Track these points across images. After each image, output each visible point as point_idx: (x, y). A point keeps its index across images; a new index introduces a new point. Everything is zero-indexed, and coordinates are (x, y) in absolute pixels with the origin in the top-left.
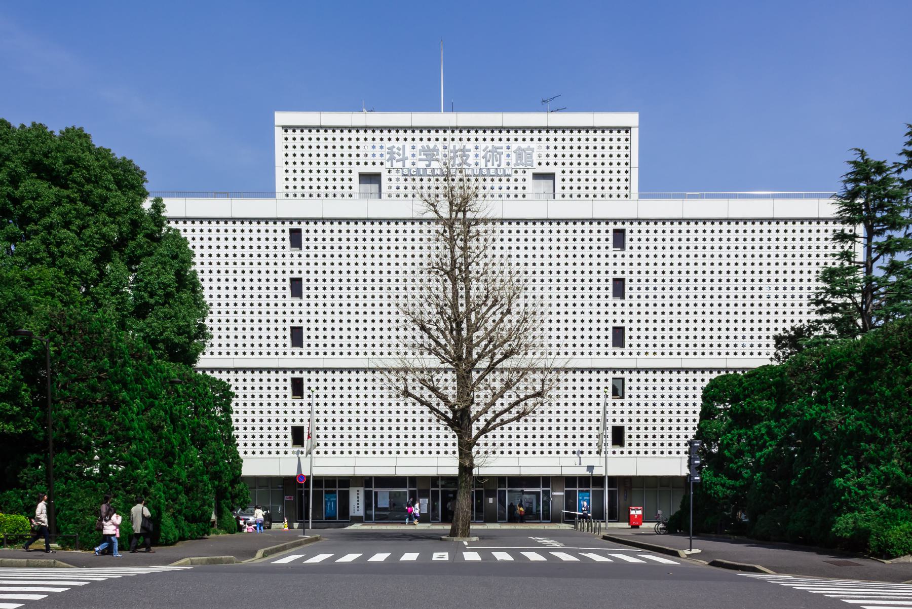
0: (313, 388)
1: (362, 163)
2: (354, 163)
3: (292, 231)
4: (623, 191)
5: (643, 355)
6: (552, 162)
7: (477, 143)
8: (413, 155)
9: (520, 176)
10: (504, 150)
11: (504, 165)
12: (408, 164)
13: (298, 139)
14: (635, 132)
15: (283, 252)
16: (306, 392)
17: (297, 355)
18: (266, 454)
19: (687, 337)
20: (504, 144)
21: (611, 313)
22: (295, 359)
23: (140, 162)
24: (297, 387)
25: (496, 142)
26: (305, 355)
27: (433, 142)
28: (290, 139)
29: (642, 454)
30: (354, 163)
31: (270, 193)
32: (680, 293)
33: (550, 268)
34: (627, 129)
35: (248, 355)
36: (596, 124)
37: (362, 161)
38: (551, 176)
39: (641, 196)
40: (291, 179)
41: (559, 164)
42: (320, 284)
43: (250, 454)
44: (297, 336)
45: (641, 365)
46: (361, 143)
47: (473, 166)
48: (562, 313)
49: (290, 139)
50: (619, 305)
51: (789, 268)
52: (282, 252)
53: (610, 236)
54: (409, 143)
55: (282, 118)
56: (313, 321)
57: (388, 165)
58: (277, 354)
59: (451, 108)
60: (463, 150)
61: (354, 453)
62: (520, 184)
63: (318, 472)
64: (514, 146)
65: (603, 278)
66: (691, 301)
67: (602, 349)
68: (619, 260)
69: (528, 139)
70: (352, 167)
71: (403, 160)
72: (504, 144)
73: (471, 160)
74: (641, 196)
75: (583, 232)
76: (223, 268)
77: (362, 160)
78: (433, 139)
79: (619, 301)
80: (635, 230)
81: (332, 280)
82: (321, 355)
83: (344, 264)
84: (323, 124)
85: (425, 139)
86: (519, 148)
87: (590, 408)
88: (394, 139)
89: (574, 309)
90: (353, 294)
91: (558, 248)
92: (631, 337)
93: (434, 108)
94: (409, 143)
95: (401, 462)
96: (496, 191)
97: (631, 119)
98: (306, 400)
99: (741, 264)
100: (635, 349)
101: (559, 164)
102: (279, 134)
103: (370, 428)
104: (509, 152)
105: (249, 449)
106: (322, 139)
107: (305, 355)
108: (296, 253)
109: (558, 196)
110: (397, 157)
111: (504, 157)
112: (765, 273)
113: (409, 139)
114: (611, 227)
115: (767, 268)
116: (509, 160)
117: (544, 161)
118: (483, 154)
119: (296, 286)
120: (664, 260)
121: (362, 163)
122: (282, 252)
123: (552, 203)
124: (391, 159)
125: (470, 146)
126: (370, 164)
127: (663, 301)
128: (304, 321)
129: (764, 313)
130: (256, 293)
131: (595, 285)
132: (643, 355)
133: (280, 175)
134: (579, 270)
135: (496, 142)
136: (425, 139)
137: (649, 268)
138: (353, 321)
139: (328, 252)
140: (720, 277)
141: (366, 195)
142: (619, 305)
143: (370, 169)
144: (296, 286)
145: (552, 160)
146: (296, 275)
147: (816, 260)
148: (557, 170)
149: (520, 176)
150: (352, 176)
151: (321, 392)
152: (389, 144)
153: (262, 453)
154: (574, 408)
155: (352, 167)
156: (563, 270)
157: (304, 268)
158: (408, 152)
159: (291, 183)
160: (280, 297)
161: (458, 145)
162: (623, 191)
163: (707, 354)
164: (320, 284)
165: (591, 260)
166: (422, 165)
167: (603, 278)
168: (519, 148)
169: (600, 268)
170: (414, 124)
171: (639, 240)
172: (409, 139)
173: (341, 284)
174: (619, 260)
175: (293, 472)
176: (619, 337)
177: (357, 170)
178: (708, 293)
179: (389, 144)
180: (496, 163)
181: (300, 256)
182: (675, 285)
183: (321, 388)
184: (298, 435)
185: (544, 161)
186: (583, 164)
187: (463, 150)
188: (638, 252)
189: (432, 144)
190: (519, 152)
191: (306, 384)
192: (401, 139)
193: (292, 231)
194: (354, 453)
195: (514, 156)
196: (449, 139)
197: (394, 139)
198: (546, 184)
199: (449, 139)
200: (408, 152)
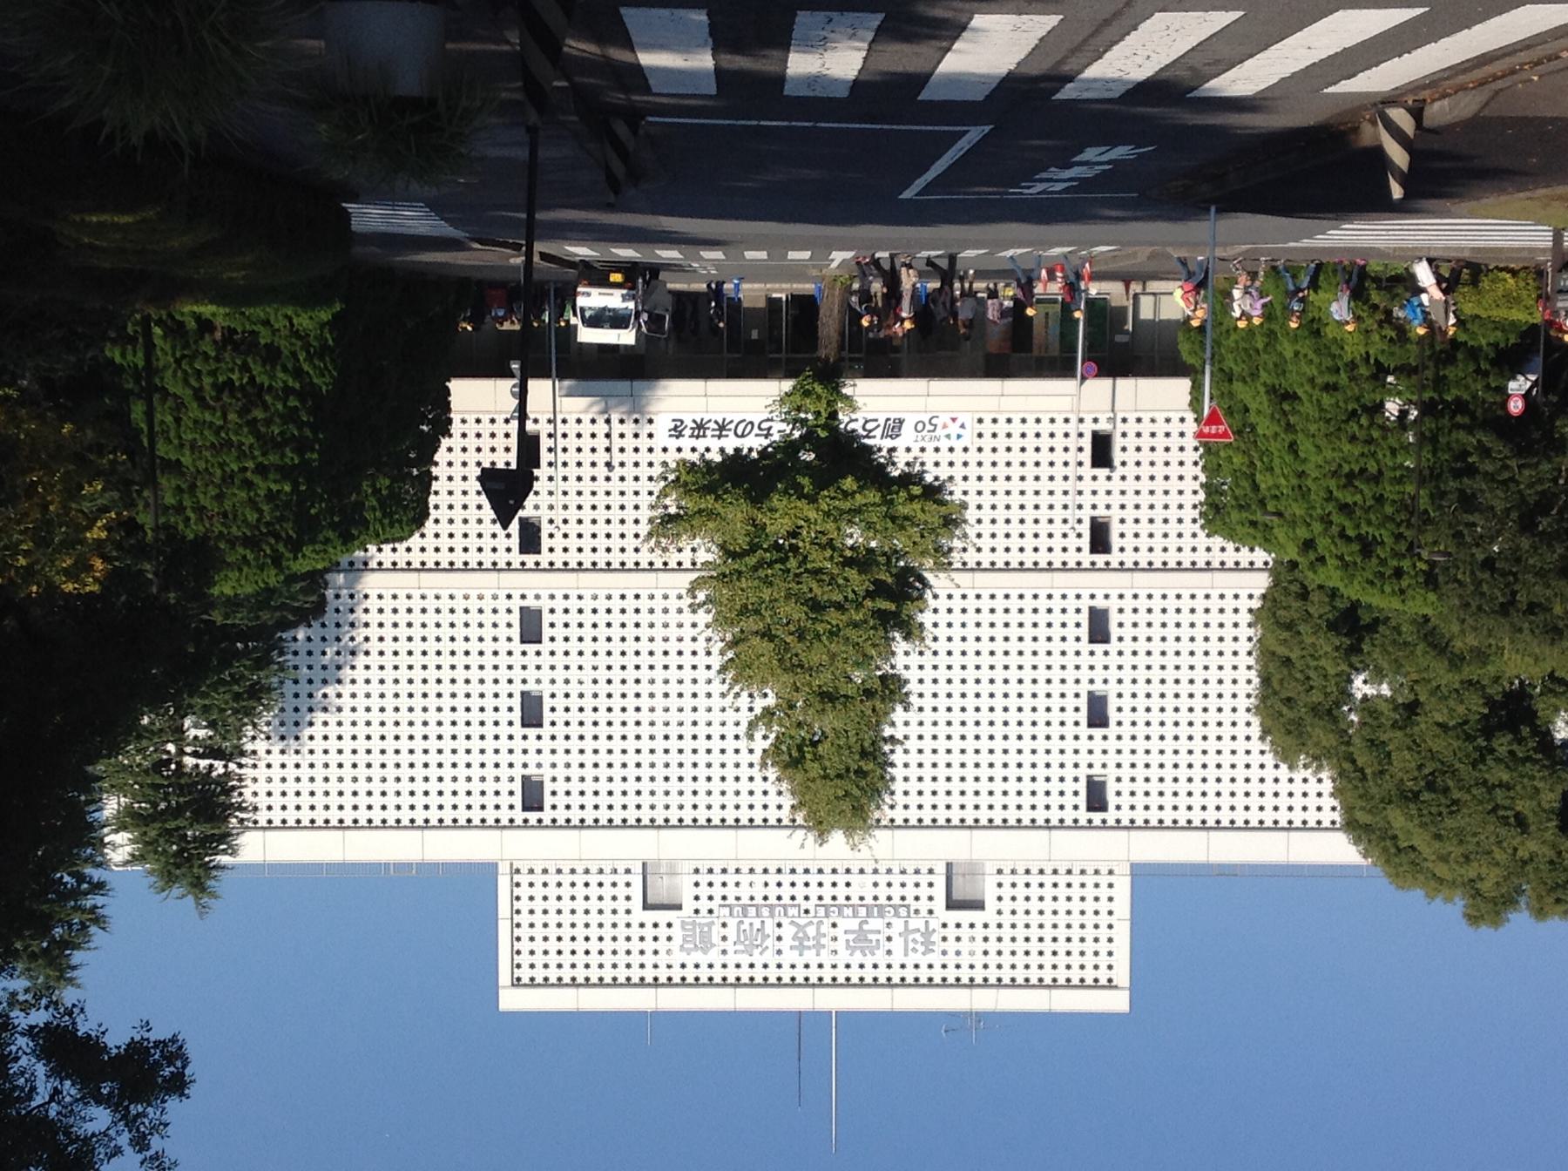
0: (1072, 535)
1: (979, 926)
2: (993, 926)
3: (1103, 807)
4: (524, 879)
5: (488, 594)
6: (965, 930)
7: (723, 959)
8: (889, 939)
9: (704, 905)
10: (731, 949)
11: (732, 923)
12: (898, 925)
13: (608, 966)
14: (504, 977)
15: (1119, 772)
16: (1085, 529)
17: (1100, 594)
18: (1160, 417)
19: (978, 695)
20: (731, 959)
21: (1228, 668)
22: (1101, 587)
23: (1541, 925)
24: (1100, 538)
25: (800, 963)
26: (1085, 594)
27: (910, 964)
28: (1103, 967)
29: (485, 419)
30: (993, 926)
31: (1141, 873)
32: (963, 703)
33: (1034, 745)
34: (517, 983)
35: (1171, 594)
36: (572, 991)
37: (979, 932)
38: (952, 905)
39: (495, 865)
40: (1007, 899)
41: (635, 925)
42: (1141, 716)
43: (1175, 417)
44: (531, 628)
45: (1045, 578)
46: (979, 960)
47: (785, 921)
48: (1099, 668)
49: (1103, 967)
50: (1098, 681)
51: (956, 786)
52: (1122, 772)
53: (548, 800)
54: (896, 960)
55: (1118, 1002)
56: (503, 653)
57: (935, 924)
58: (552, 597)
59: (820, 1018)
60: (801, 949)
61: (1002, 419)
62: (704, 891)
63: (1066, 386)
64: (714, 956)
65: (1126, 727)
66: (1156, 688)
67: (559, 604)
68: (1097, 759)
69: (690, 966)
70: (995, 919)
71: (907, 930)
72: (731, 959)
73: (788, 931)
74: (495, 865)
75: (1147, 808)
76: (1055, 744)
77: (979, 932)
78: (910, 968)
79: (1098, 687)
80: (1069, 811)
81: (1006, 723)
82: (1143, 594)
83: (998, 751)
84: (1045, 992)
85: (869, 966)
86: (705, 951)
87: (594, 500)
88: (923, 967)
89: (1178, 674)
90: (1141, 699)
91: (1062, 779)
92: (509, 625)
93: (848, 1019)
94: (896, 960)
95: (992, 403)
96: (759, 879)
97: (511, 1000)
98: (1086, 514)
99: (376, 752)
100: (502, 604)
101: (635, 925)
102: (1122, 975)
103: (987, 464)
104: (723, 946)
105: (1175, 428)
106: (580, 966)
107: (1085, 594)
108: (1097, 770)
109: (941, 869)
110: (918, 936)
111: (732, 937)
112: (1013, 737)
113: (896, 966)
114: (547, 816)
115: (358, 745)
116: (724, 931)
117: (663, 932)
118: (769, 942)
119: (1098, 715)
120: (1020, 716)
121: (979, 926)
122: (1122, 772)
123: (650, 854)
124: (928, 933)
125: (789, 957)
126: (663, 925)
127: (1063, 688)
128: (517, 653)
129: (1085, 668)
130: (1213, 703)
131: (489, 716)
132: (488, 594)
133: (1123, 906)
134: (1169, 742)
135: (800, 963)
136: (869, 966)
137: (1002, 744)
138: (956, 653)
139: (702, 772)
140: (624, 730)
141: (974, 870)
142: (1098, 681)
143: (965, 916)
144: (1098, 715)
145: (649, 932)
146: (532, 732)
147: (315, 758)
148: (639, 914)
149: (704, 905)
150: (996, 905)
151: (1058, 528)
152: (930, 958)
153: (1139, 420)
154: (594, 500)
155: (995, 919)
156: (1169, 742)
157: (1084, 744)
158: (897, 945)
159: (704, 891)
160: (1127, 695)
161: (810, 957)
162: (524, 879)
163: (616, 596)
164: (574, 716)
165: (1163, 675)
166: (875, 923)
167: (1126, 727)
168: (705, 951)
169: (1045, 745)
170: (888, 991)
171: (312, 794)
172: (896, 966)
173: (1006, 716)
174: (1097, 759)
175: (1125, 384)
176: (531, 628)
177: (988, 915)
178: (1042, 702)
179: (930, 958)
180: (746, 926)
181: (525, 766)
182: (1042, 702)
183: (1058, 535)
184: (1102, 452)
185: (663, 932)
186: (1169, 737)
187: (801, 949)
188: (1065, 772)
189: (857, 958)
190: (706, 946)
191: (1085, 542)
192: (855, 967)
193: (1103, 807)
194: (1002, 419)
195: (716, 939)
196: (827, 967)
197: (923, 967)
198: (657, 894)
199: (827, 967)
200: (897, 945)
